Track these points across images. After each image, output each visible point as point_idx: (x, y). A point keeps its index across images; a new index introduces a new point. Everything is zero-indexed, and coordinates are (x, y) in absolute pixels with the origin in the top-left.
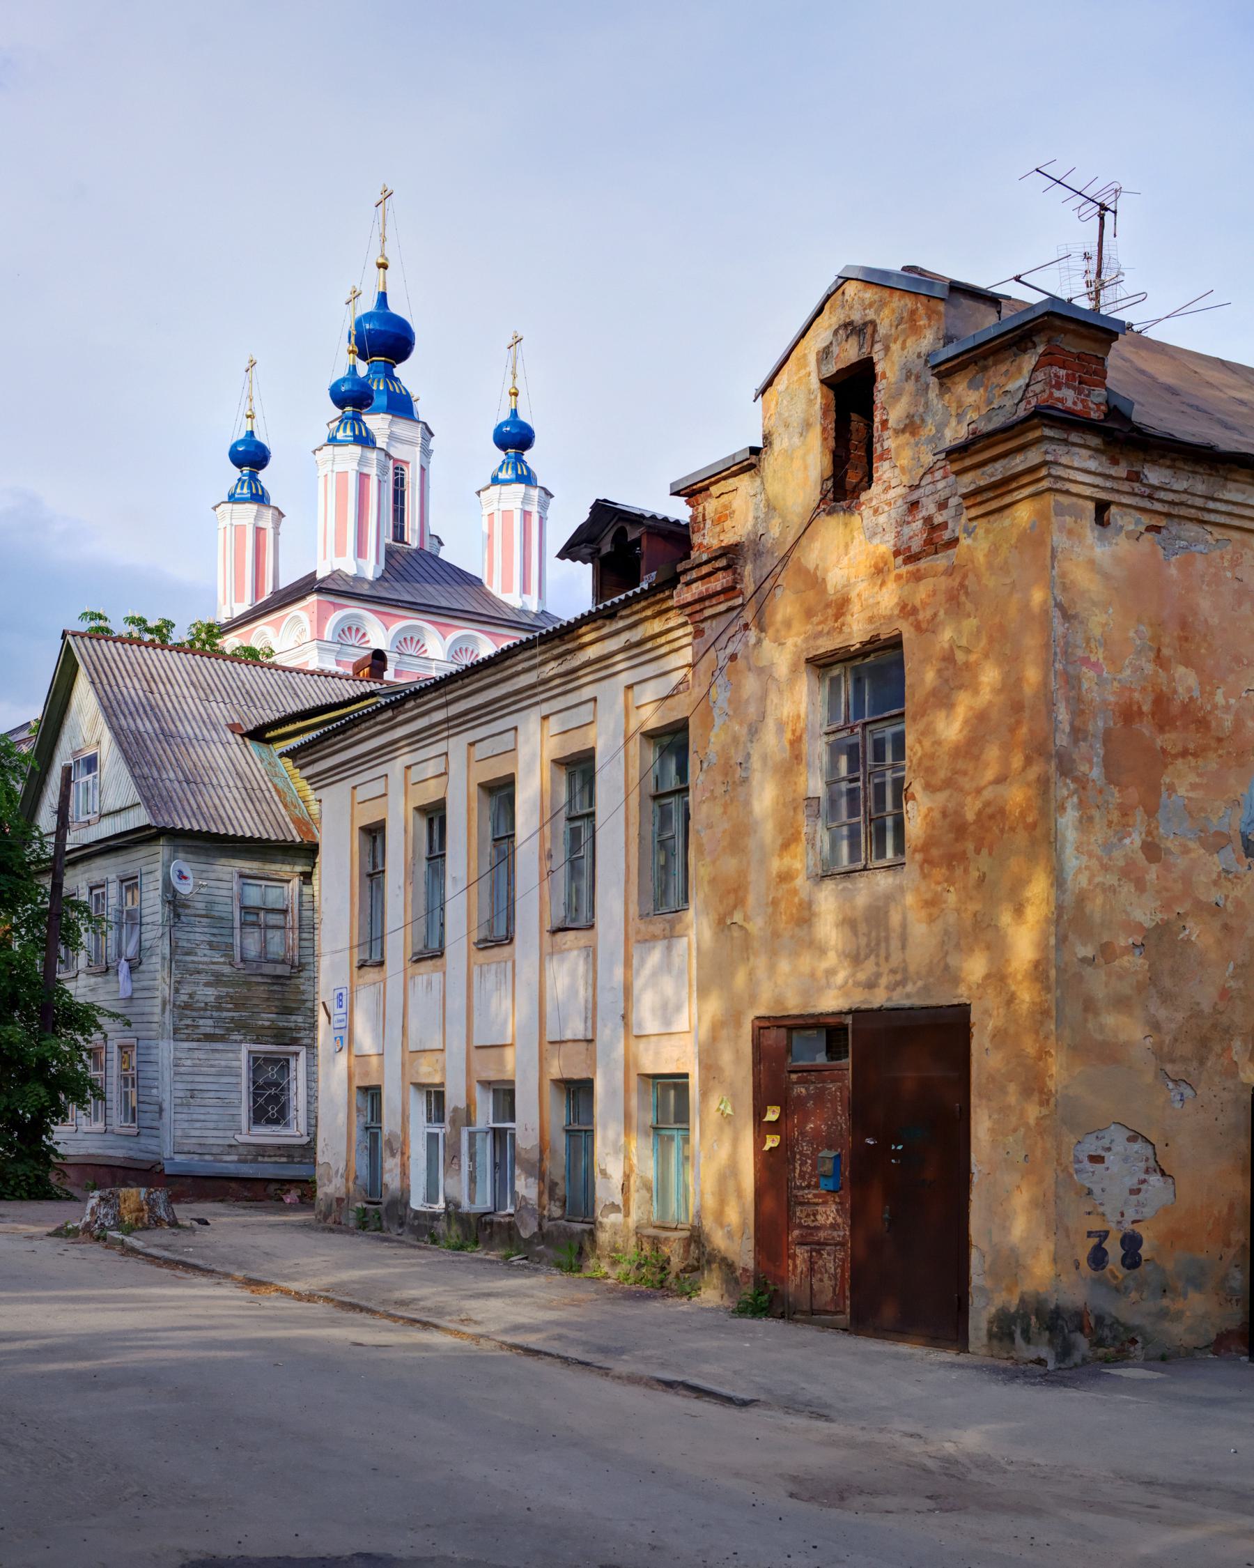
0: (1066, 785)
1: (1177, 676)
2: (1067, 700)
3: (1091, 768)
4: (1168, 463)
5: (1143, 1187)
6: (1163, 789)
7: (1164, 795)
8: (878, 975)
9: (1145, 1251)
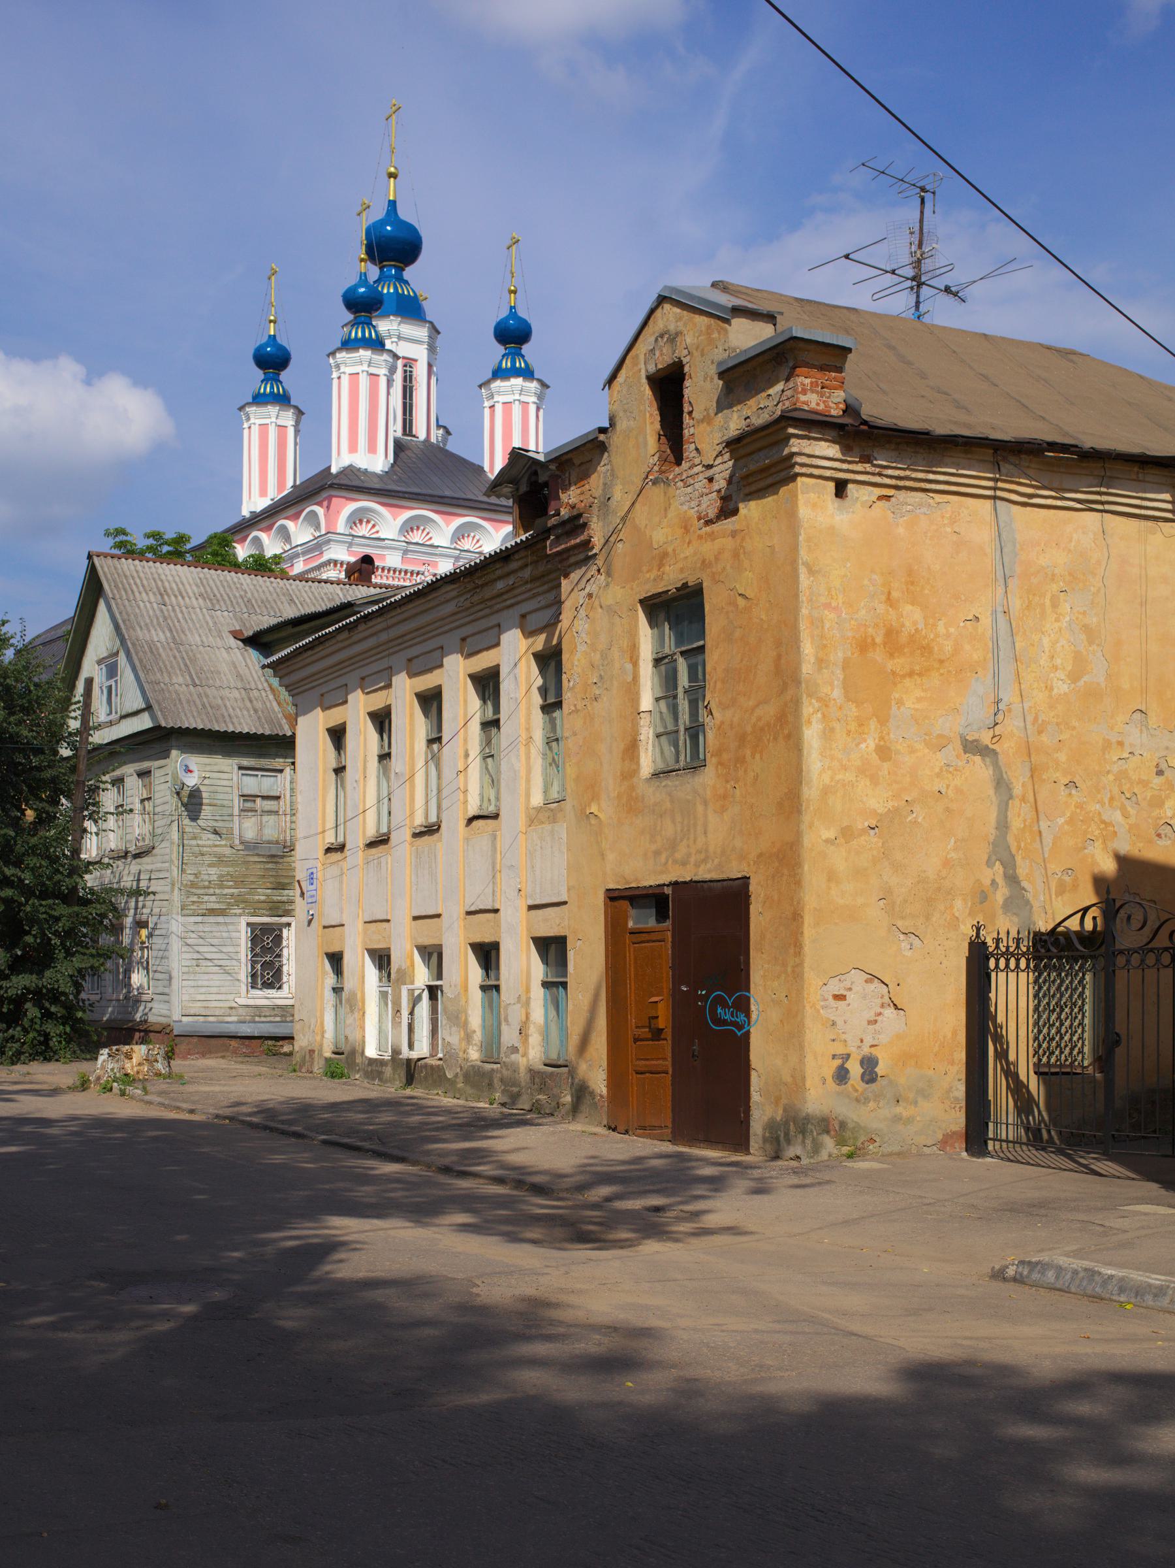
0: (811, 704)
1: (904, 613)
2: (812, 637)
3: (832, 690)
4: (893, 446)
5: (879, 1018)
6: (893, 703)
7: (894, 708)
8: (689, 855)
9: (880, 1070)
